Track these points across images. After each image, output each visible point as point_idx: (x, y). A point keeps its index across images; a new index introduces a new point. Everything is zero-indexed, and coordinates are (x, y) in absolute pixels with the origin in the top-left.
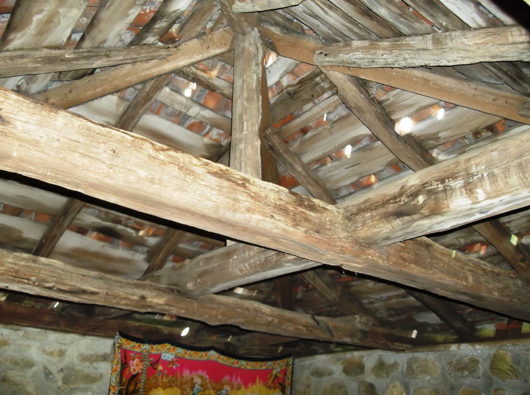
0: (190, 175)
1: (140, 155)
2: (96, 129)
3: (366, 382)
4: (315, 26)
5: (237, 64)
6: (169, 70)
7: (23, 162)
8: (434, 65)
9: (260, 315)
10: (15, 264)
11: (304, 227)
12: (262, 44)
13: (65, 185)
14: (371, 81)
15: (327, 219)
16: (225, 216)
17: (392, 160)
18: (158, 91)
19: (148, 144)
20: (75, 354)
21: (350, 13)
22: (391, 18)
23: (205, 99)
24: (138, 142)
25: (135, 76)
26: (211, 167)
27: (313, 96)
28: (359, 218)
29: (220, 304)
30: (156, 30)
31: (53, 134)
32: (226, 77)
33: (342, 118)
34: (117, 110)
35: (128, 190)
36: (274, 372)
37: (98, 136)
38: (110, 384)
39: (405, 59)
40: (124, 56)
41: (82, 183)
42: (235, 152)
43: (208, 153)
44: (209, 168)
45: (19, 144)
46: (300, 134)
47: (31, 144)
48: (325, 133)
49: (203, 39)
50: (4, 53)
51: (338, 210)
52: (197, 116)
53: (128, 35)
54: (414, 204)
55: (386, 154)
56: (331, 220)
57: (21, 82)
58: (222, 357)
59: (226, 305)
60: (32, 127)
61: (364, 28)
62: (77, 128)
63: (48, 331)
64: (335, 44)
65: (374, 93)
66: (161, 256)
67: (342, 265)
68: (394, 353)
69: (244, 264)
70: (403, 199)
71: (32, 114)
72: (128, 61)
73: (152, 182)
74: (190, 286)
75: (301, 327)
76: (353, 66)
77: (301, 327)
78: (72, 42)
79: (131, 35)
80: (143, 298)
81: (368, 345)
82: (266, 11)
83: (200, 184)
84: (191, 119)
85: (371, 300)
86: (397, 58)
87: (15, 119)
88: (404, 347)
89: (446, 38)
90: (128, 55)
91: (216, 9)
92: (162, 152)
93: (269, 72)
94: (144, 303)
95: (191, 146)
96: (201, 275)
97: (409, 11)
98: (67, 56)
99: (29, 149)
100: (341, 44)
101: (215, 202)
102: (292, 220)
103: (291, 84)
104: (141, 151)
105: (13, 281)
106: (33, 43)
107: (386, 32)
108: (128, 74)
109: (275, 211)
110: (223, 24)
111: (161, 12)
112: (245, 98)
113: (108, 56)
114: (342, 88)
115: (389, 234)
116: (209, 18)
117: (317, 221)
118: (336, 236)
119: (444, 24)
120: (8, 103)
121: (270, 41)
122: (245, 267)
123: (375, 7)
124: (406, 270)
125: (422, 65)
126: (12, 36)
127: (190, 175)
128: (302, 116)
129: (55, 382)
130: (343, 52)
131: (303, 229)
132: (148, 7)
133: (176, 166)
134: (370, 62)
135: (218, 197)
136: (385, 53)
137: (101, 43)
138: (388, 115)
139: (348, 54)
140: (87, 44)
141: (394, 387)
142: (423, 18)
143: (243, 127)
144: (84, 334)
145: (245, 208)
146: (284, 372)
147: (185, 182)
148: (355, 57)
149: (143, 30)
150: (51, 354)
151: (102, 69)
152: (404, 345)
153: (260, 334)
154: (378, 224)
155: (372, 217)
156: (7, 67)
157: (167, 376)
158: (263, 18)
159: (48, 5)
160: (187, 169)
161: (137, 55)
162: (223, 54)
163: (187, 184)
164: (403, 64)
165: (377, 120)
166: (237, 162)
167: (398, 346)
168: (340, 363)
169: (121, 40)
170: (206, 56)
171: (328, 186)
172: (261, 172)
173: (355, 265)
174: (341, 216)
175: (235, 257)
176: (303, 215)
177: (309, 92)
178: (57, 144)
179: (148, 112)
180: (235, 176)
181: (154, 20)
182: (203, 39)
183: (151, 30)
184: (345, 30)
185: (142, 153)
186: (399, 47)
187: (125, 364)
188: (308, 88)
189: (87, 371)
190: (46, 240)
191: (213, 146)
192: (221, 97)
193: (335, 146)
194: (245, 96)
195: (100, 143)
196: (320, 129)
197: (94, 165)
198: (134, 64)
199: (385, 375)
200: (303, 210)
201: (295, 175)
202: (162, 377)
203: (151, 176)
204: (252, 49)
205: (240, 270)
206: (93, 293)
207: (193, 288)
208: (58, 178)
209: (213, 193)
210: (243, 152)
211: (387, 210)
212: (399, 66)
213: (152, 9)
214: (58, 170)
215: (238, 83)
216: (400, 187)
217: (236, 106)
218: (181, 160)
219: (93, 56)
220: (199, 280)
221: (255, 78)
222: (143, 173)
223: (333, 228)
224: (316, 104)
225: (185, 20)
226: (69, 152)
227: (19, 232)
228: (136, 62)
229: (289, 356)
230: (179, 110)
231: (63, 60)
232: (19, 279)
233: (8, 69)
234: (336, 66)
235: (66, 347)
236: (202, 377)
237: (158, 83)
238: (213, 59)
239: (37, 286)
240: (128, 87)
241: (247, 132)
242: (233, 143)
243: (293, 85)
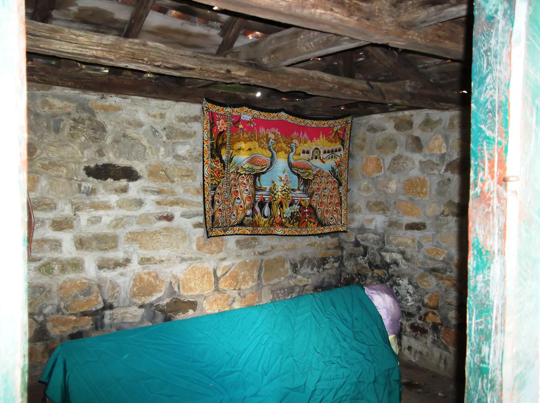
3: (413, 136)
9: (323, 82)
10: (131, 48)
11: (357, 16)
15: (376, 8)
20: (173, 116)
29: (289, 74)
36: (335, 129)
38: (203, 139)
58: (291, 117)
59: (295, 75)
63: (149, 99)
66: (233, 30)
67: (388, 44)
68: (440, 112)
69: (309, 43)
74: (265, 60)
75: (357, 92)
77: (357, 92)
80: (228, 71)
81: (416, 105)
85: (426, 65)
88: (448, 106)
94: (229, 76)
96: (274, 52)
105: (132, 62)
115: (426, 19)
118: (383, 22)
122: (310, 45)
124: (441, 45)
129: (162, 137)
131: (356, 18)
141: (436, 139)
144: (177, 101)
145: (310, 5)
146: (344, 129)
150: (154, 116)
152: (448, 105)
153: (323, 98)
154: (417, 11)
155: (413, 5)
157: (247, 133)
167: (443, 106)
168: (392, 121)
173: (399, 43)
174: (388, 4)
175: (302, 37)
176: (357, 6)
187: (213, 124)
189: (183, 129)
190: (134, 21)
199: (430, 130)
202: (243, 134)
205: (306, 48)
206: (191, 69)
207: (268, 62)
220: (272, 56)
223: (381, 15)
229: (349, 115)
232: (136, 60)
235: (165, 111)
236: (275, 134)
239: (149, 65)
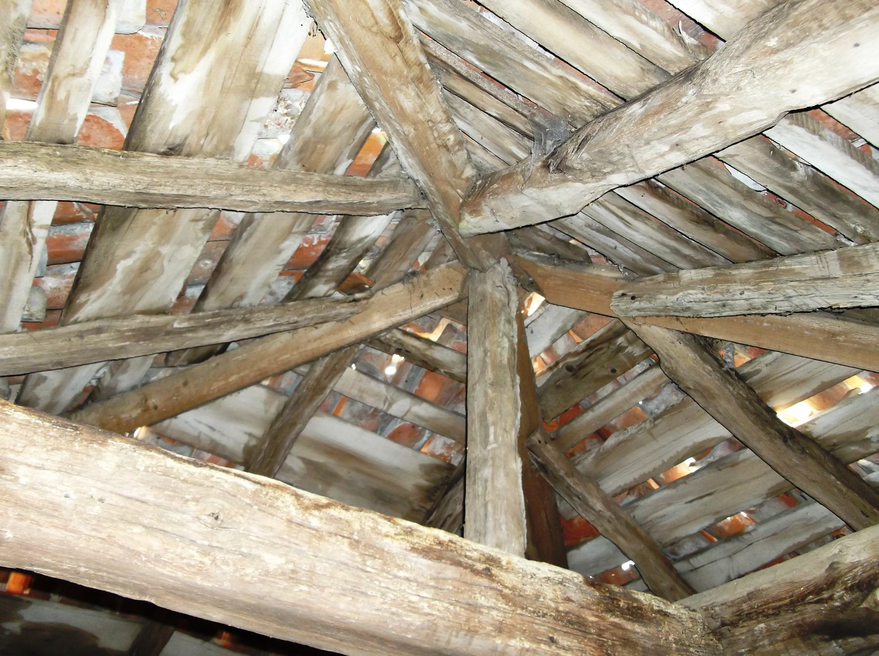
0: (375, 558)
1: (270, 522)
2: (181, 471)
4: (610, 250)
5: (473, 322)
6: (353, 339)
7: (28, 549)
8: (849, 305)
12: (517, 286)
13: (117, 591)
14: (721, 340)
16: (451, 646)
17: (778, 485)
18: (336, 374)
19: (288, 496)
21: (672, 221)
22: (753, 226)
23: (420, 384)
24: (267, 494)
25: (295, 353)
26: (419, 537)
27: (614, 371)
28: (742, 634)
30: (330, 273)
31: (92, 489)
32: (455, 346)
33: (671, 410)
34: (266, 412)
35: (242, 598)
37: (184, 485)
39: (788, 298)
40: (275, 320)
41: (150, 587)
42: (475, 483)
43: (427, 480)
44: (415, 540)
45: (19, 515)
46: (595, 440)
47: (42, 514)
48: (640, 436)
49: (412, 283)
50: (69, 327)
51: (692, 614)
52: (406, 414)
53: (284, 284)
54: (867, 609)
55: (765, 474)
56: (680, 640)
57: (102, 371)
60: (49, 477)
61: (700, 247)
62: (144, 473)
64: (647, 278)
65: (728, 360)
70: (837, 595)
71: (52, 450)
72: (282, 328)
73: (293, 579)
76: (686, 314)
78: (187, 301)
79: (289, 283)
82: (518, 228)
83: (395, 576)
84: (397, 421)
86: (772, 296)
87: (16, 462)
89: (866, 254)
90: (282, 316)
91: (432, 232)
92: (316, 513)
93: (532, 332)
95: (398, 468)
97: (788, 212)
98: (176, 325)
99: (38, 524)
100: (660, 277)
101: (428, 614)
102: (594, 645)
103: (572, 350)
104: (271, 510)
106: (118, 307)
107: (744, 251)
108: (285, 349)
109: (558, 628)
110: (445, 255)
111: (337, 242)
112: (488, 382)
113: (246, 321)
114: (668, 355)
116: (421, 247)
117: (649, 644)
119: (860, 230)
120: (7, 431)
121: (531, 279)
123: (720, 209)
125: (824, 306)
126: (82, 298)
127: (375, 558)
128: (596, 408)
130: (664, 291)
132: (316, 237)
133: (346, 540)
134: (718, 306)
135: (433, 602)
136: (746, 289)
137: (235, 301)
138: (762, 401)
139: (675, 293)
140: (212, 303)
142: (816, 221)
143: (487, 436)
145: (492, 625)
147: (363, 575)
148: (687, 299)
149: (308, 275)
151: (241, 342)
156: (72, 350)
158: (515, 241)
159: (142, 243)
160: (368, 546)
161: (298, 316)
162: (447, 305)
163: (368, 577)
164: (785, 306)
165: (740, 410)
166: (479, 503)
169: (272, 293)
170: (418, 310)
171: (655, 536)
172: (525, 521)
174: (699, 629)
176: (620, 633)
177: (605, 365)
178: (96, 509)
179: (319, 412)
180: (468, 554)
181: (325, 257)
182: (412, 283)
183: (321, 274)
184: (665, 252)
185: (273, 516)
186: (774, 277)
188: (604, 358)
191: (438, 467)
192: (447, 380)
193: (663, 461)
194: (490, 379)
195: (187, 501)
196: (632, 430)
197: (172, 550)
198: (295, 332)
200: (617, 620)
201: (590, 518)
203: (291, 566)
204: (499, 295)
208: (102, 577)
209: (424, 594)
210: (489, 484)
211: (803, 619)
212: (777, 312)
213: (323, 239)
214: (99, 564)
215: (476, 354)
216: (827, 566)
217: (473, 397)
218: (356, 526)
219: (222, 323)
221: (506, 345)
222: (274, 561)
224: (620, 386)
225: (379, 253)
226: (121, 525)
227: (93, 637)
228: (295, 329)
230: (374, 406)
231: (168, 333)
233: (72, 353)
234: (653, 316)
237: (335, 361)
238: (431, 315)
240: (285, 371)
241: (495, 445)
242: (470, 466)
243: (576, 354)
